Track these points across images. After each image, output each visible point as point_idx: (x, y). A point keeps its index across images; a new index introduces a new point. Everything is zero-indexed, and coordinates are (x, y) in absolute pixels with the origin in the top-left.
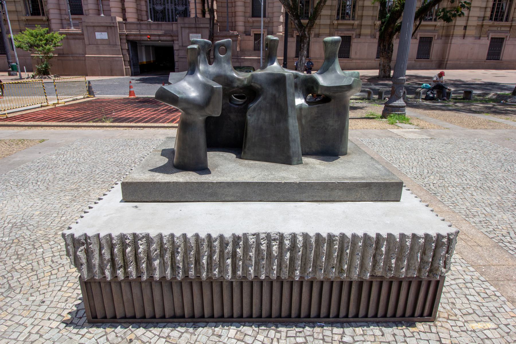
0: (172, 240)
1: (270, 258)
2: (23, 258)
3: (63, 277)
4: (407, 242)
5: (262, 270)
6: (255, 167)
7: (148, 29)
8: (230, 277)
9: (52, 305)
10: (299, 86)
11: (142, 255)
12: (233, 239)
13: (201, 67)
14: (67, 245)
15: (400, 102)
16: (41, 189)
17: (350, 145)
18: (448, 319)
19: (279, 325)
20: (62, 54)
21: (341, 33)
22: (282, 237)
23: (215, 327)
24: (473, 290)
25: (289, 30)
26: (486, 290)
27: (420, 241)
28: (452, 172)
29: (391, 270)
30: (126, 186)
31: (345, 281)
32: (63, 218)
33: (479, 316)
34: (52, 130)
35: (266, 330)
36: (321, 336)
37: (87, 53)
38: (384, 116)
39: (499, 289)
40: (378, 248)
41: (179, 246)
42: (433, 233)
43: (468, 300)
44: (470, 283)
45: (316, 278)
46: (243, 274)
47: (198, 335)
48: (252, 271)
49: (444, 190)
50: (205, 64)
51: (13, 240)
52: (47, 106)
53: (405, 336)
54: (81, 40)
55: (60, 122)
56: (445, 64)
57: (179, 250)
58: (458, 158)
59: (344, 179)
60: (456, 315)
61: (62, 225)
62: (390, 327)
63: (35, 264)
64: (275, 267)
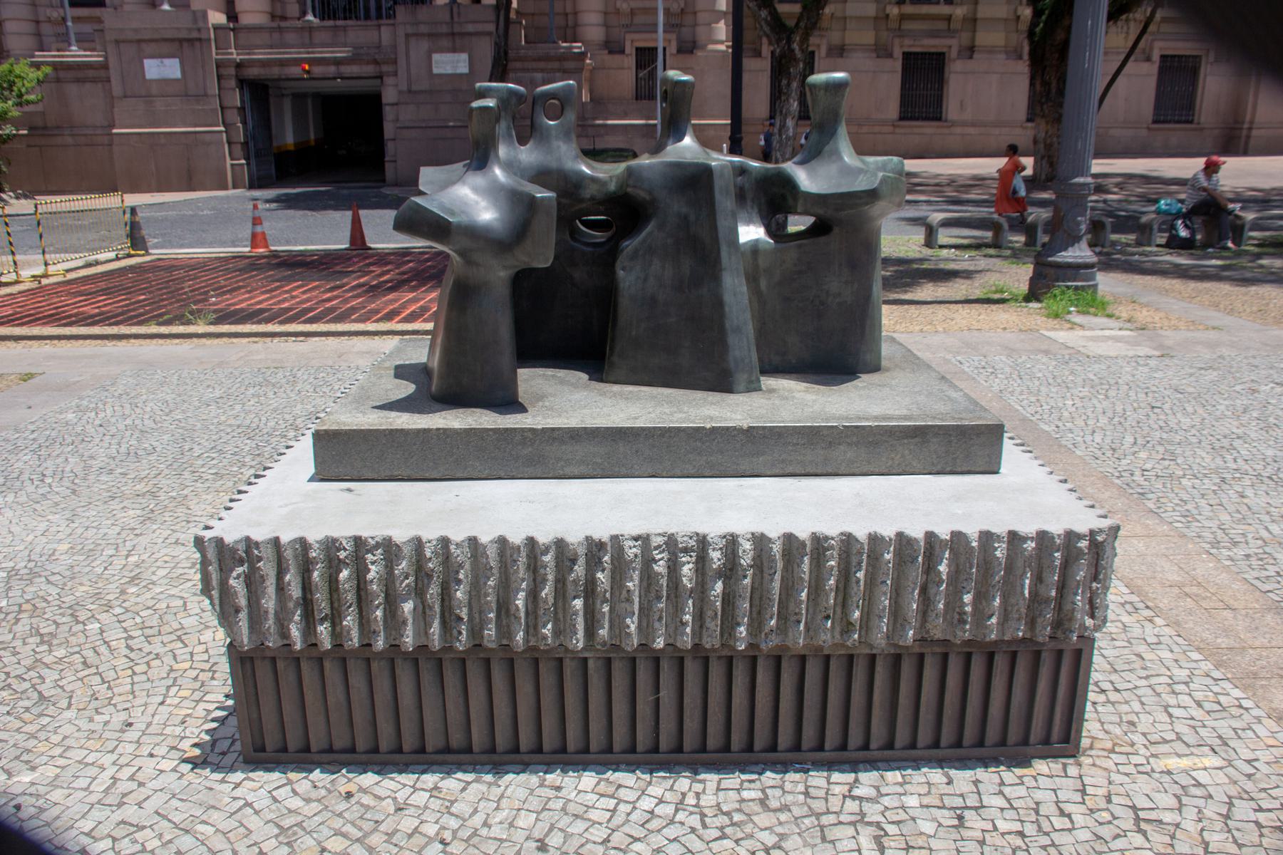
0: (443, 554)
1: (676, 597)
2: (55, 642)
3: (163, 678)
4: (996, 549)
5: (657, 625)
6: (639, 399)
7: (303, 46)
8: (580, 645)
9: (150, 730)
10: (750, 195)
11: (375, 587)
12: (588, 549)
13: (503, 151)
14: (205, 563)
15: (1080, 253)
16: (57, 493)
17: (886, 350)
18: (1113, 751)
19: (700, 770)
20: (39, 129)
21: (911, 42)
22: (703, 542)
23: (546, 772)
24: (1187, 698)
25: (748, 36)
26: (1219, 697)
27: (1025, 546)
28: (1200, 442)
29: (965, 622)
30: (324, 441)
31: (858, 655)
32: (132, 559)
33: (1188, 745)
34: (47, 348)
35: (670, 778)
36: (801, 788)
37: (117, 122)
38: (1033, 295)
39: (1254, 694)
40: (930, 567)
41: (461, 566)
42: (1056, 528)
43: (1170, 716)
44: (1184, 683)
45: (788, 648)
46: (611, 639)
47: (507, 787)
48: (633, 627)
49: (1169, 486)
50: (510, 143)
51: (20, 605)
52: (17, 282)
53: (1002, 783)
54: (100, 85)
55: (65, 325)
56: (1243, 140)
57: (461, 576)
58: (1227, 406)
59: (859, 419)
60: (1133, 744)
61: (133, 574)
62: (970, 769)
63: (89, 654)
64: (688, 618)
